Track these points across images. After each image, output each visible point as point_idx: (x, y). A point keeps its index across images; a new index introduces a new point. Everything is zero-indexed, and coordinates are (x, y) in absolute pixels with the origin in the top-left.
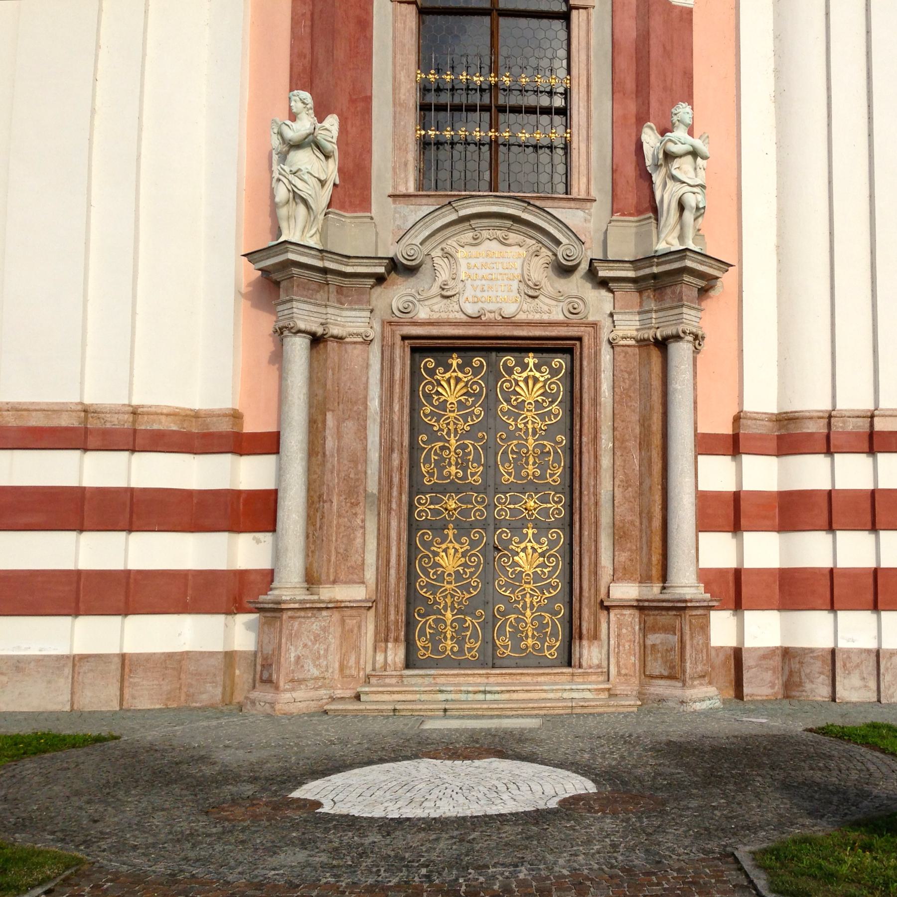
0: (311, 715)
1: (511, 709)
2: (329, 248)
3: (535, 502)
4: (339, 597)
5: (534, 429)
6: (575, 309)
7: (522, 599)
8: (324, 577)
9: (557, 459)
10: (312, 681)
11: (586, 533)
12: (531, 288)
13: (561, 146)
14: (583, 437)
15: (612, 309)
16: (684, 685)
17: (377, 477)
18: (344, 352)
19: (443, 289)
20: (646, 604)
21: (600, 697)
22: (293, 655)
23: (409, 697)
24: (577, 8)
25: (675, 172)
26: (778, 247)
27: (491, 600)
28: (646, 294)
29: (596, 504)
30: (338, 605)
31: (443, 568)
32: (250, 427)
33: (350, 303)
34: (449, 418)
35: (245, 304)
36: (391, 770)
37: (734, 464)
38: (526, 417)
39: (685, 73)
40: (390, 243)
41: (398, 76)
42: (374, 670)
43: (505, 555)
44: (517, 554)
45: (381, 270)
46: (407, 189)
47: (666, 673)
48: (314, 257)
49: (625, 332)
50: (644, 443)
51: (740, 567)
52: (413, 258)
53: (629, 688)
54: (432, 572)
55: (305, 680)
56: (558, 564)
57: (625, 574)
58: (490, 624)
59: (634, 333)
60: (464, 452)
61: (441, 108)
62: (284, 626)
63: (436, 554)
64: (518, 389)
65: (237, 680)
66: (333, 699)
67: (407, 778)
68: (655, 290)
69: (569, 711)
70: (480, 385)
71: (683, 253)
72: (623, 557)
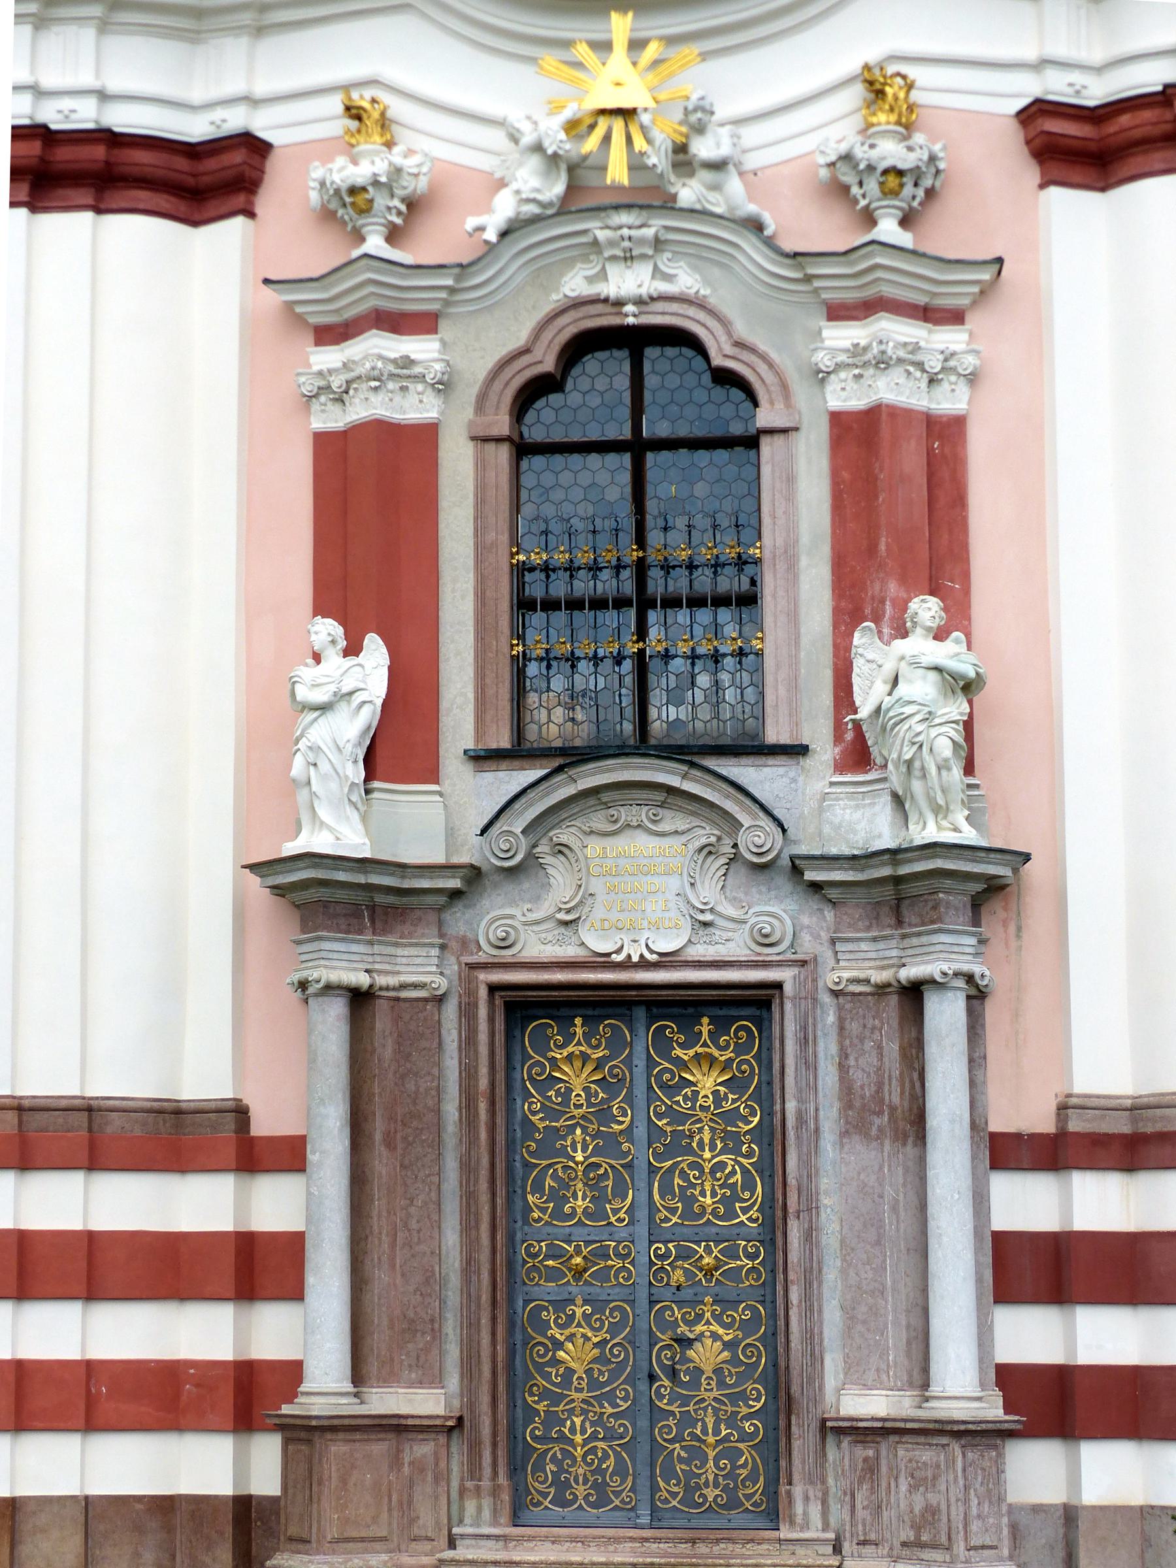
61: (551, 605)
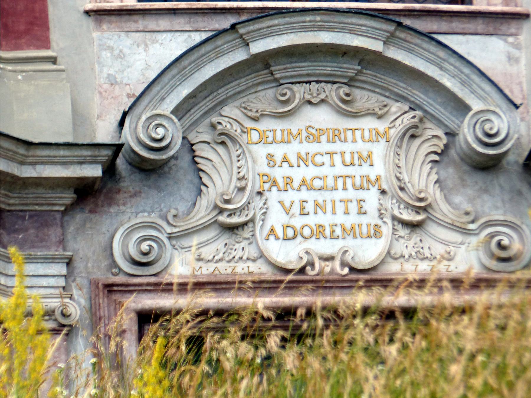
19: (221, 211)
52: (163, 144)
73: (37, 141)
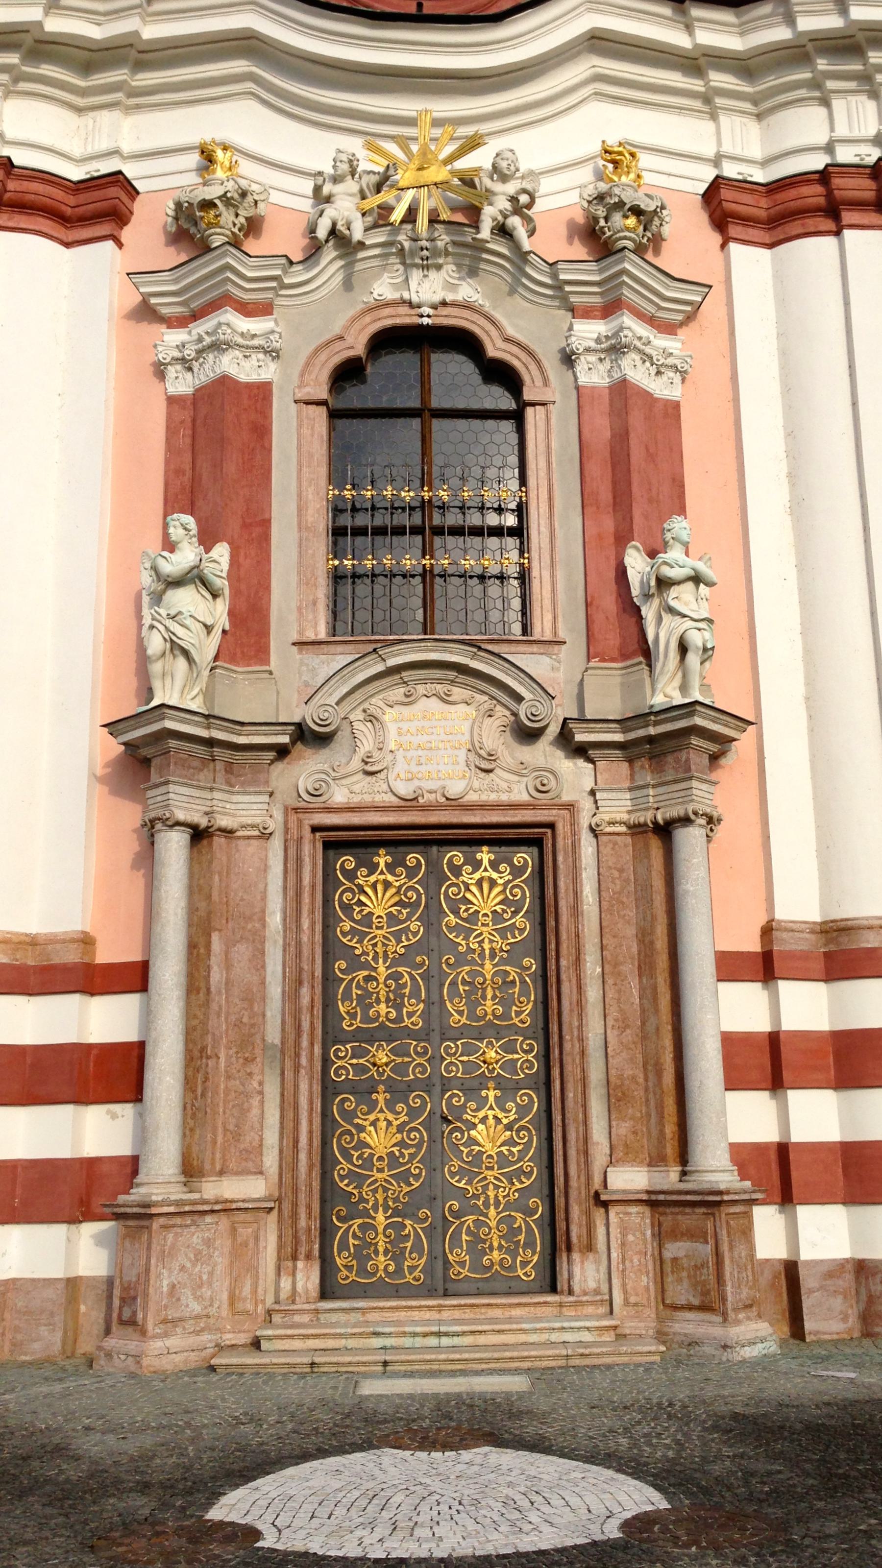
0: (193, 1373)
1: (480, 1360)
2: (216, 712)
3: (497, 1052)
4: (228, 1195)
5: (492, 950)
6: (543, 785)
7: (484, 1192)
8: (207, 1166)
9: (524, 992)
10: (192, 1322)
11: (570, 1095)
12: (484, 759)
13: (516, 575)
14: (562, 960)
15: (593, 784)
16: (725, 1320)
17: (279, 1021)
18: (234, 850)
19: (366, 763)
20: (661, 1197)
21: (603, 1339)
22: (165, 1283)
23: (331, 1343)
24: (533, 404)
25: (673, 603)
26: (807, 699)
27: (439, 1194)
28: (638, 764)
29: (583, 1053)
30: (228, 1206)
31: (371, 1148)
32: (104, 956)
33: (242, 784)
34: (375, 937)
35: (100, 790)
36: (342, 1469)
37: (766, 993)
38: (481, 934)
39: (674, 480)
40: (295, 704)
41: (304, 494)
42: (277, 1302)
43: (457, 1129)
44: (474, 1126)
45: (285, 739)
46: (316, 635)
47: (696, 1302)
48: (197, 724)
49: (613, 816)
50: (645, 966)
51: (784, 1141)
53: (642, 1325)
54: (356, 1154)
55: (181, 1320)
56: (530, 1141)
57: (627, 1154)
58: (440, 1230)
59: (625, 817)
60: (398, 984)
62: (154, 1240)
63: (361, 1129)
64: (468, 896)
65: (82, 1320)
66: (221, 1348)
67: (371, 1484)
68: (650, 759)
69: (562, 1363)
70: (417, 892)
71: (691, 708)
72: (623, 1129)
73: (246, 721)
